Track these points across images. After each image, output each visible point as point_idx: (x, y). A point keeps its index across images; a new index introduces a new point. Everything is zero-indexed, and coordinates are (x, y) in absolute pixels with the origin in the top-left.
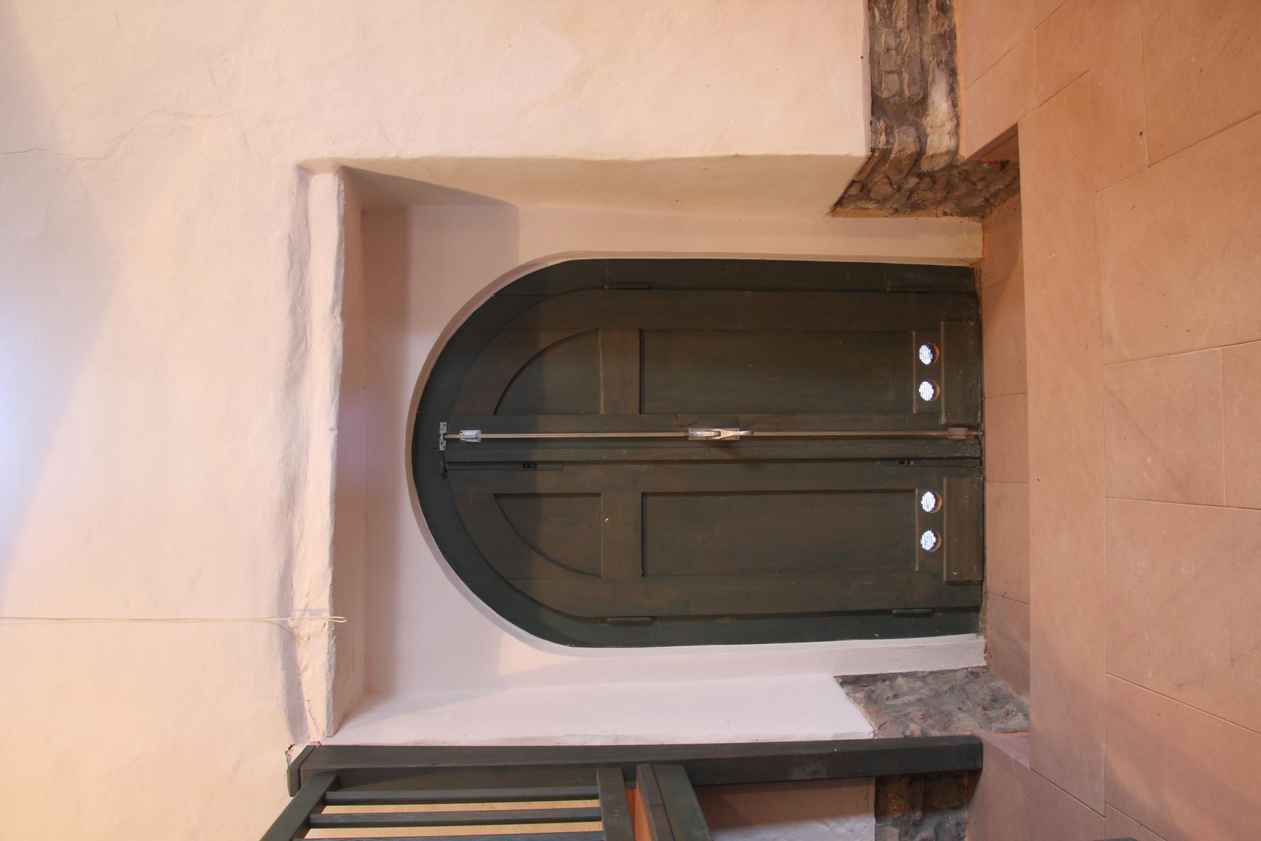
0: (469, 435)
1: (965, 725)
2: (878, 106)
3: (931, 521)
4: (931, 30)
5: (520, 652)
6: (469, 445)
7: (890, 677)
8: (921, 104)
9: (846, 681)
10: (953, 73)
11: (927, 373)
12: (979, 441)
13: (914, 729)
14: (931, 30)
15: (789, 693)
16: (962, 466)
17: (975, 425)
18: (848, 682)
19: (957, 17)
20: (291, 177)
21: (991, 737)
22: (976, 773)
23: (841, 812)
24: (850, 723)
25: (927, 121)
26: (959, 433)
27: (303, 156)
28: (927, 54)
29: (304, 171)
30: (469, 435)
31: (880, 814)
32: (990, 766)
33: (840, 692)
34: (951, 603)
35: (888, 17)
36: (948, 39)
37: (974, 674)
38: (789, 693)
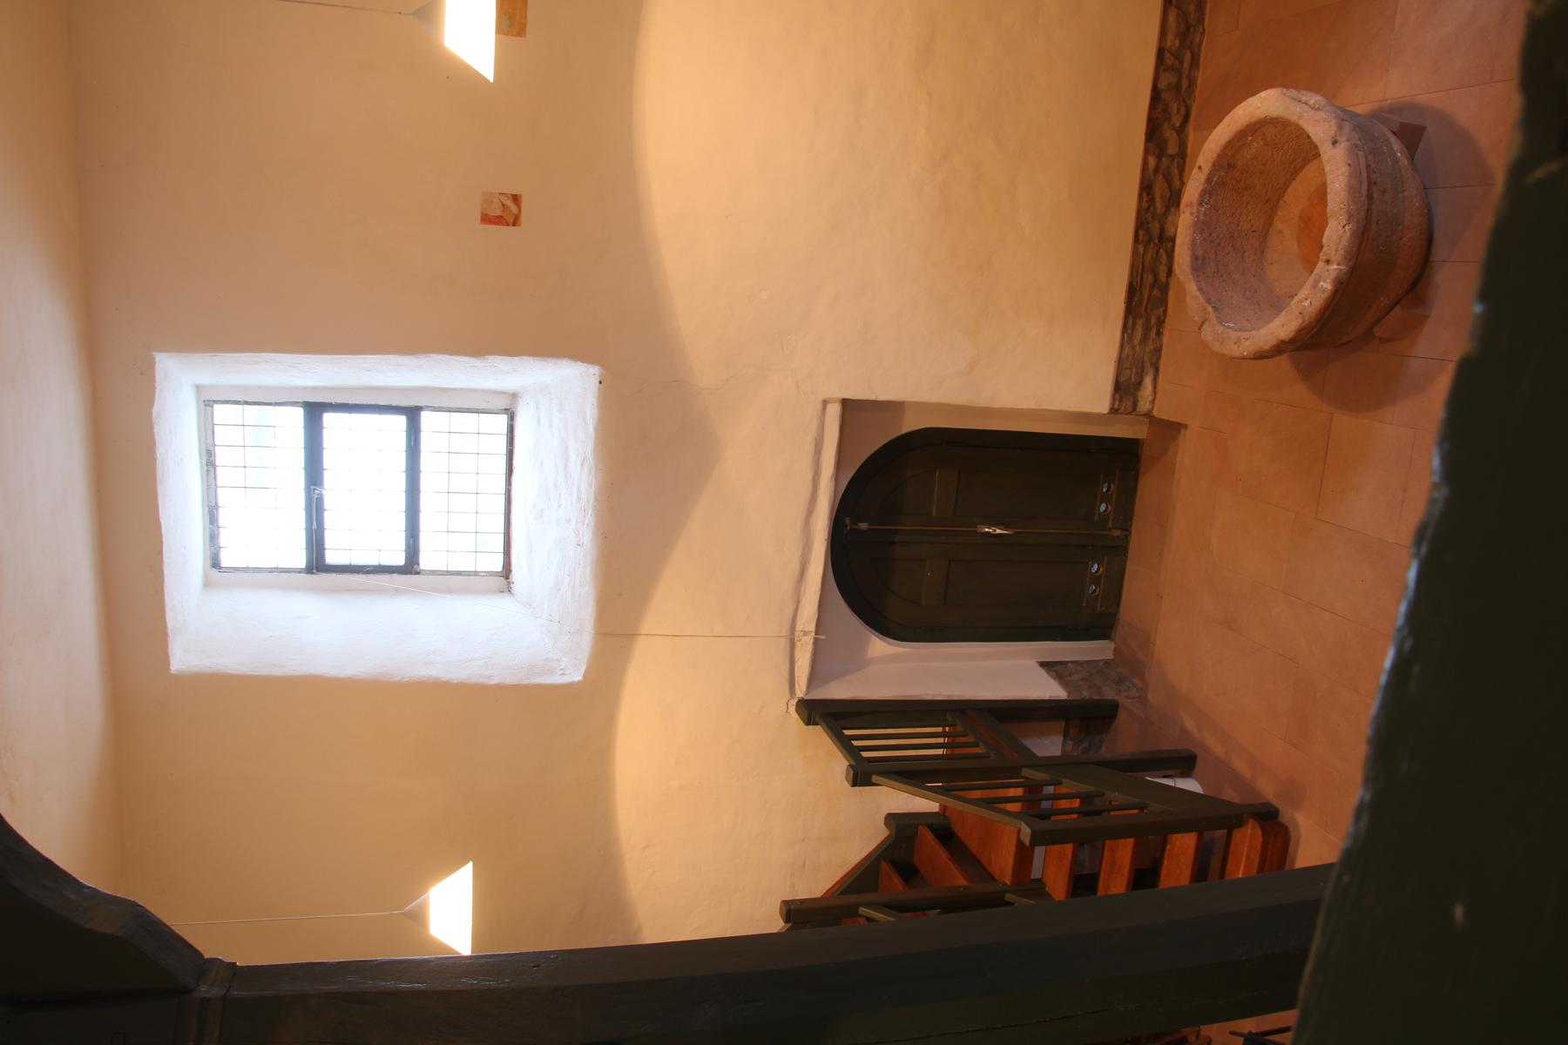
0: (863, 526)
1: (1109, 693)
2: (1118, 387)
3: (1096, 579)
4: (1150, 346)
5: (879, 646)
6: (863, 532)
7: (1061, 663)
8: (1139, 384)
9: (1043, 664)
10: (1157, 370)
11: (1105, 498)
12: (1127, 538)
13: (1086, 695)
14: (1150, 346)
15: (1009, 672)
16: (1117, 551)
17: (1127, 530)
18: (1045, 665)
19: (1165, 339)
20: (819, 406)
21: (1121, 699)
22: (1113, 717)
23: (183, 667)
24: (1049, 689)
25: (1140, 393)
26: (1117, 533)
27: (826, 397)
28: (1146, 358)
29: (825, 403)
30: (863, 526)
31: (1065, 736)
32: (1122, 716)
33: (1042, 671)
34: (1100, 625)
35: (1130, 338)
36: (1158, 351)
37: (1107, 663)
38: (1009, 672)
